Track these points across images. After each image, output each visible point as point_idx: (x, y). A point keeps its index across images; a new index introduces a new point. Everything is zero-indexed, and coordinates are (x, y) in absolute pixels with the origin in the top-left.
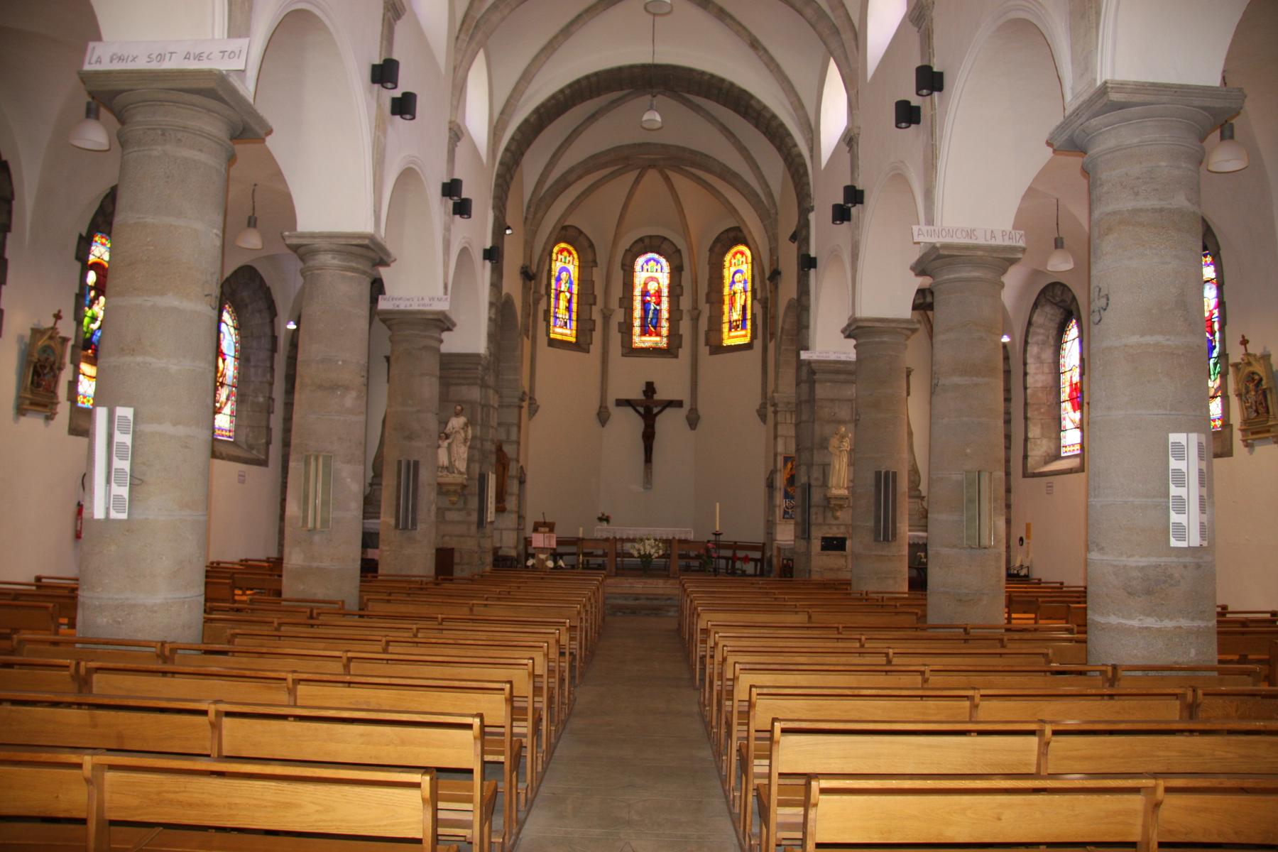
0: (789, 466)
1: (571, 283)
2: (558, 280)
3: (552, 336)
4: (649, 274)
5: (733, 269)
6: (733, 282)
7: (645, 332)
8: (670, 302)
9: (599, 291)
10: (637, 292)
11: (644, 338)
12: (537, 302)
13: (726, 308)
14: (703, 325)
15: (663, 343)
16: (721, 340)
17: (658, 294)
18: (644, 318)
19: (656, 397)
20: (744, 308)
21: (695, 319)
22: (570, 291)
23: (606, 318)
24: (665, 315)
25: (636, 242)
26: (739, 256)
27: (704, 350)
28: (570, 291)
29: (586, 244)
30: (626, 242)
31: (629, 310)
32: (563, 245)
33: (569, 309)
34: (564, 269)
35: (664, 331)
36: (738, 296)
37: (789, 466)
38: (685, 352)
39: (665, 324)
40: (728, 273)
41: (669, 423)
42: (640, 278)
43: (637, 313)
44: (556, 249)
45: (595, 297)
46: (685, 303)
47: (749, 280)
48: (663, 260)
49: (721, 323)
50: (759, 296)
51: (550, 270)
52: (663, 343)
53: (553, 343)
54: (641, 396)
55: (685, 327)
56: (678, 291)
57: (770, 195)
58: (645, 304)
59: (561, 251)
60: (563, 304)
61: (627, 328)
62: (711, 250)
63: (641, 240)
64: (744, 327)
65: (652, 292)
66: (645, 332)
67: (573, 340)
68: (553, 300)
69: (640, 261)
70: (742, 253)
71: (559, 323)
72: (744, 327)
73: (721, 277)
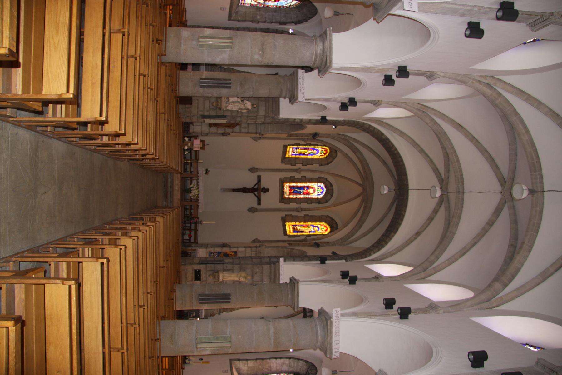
0: (233, 254)
2: (313, 149)
3: (288, 147)
4: (316, 189)
5: (319, 226)
6: (314, 226)
8: (304, 199)
9: (309, 167)
10: (309, 184)
12: (303, 140)
14: (295, 214)
15: (286, 196)
16: (288, 222)
17: (308, 193)
18: (297, 187)
19: (262, 193)
20: (302, 232)
22: (309, 154)
23: (297, 171)
24: (299, 197)
25: (331, 183)
26: (325, 229)
27: (283, 214)
28: (309, 154)
29: (329, 161)
30: (330, 179)
31: (301, 181)
32: (328, 151)
33: (301, 154)
34: (318, 151)
35: (291, 196)
36: (308, 229)
37: (233, 254)
38: (282, 206)
39: (295, 196)
40: (317, 224)
41: (250, 200)
42: (315, 185)
43: (299, 184)
44: (327, 148)
46: (304, 205)
48: (322, 195)
50: (307, 238)
51: (317, 145)
52: (286, 196)
53: (285, 147)
55: (293, 205)
57: (352, 242)
58: (303, 188)
59: (326, 150)
60: (303, 151)
61: (292, 180)
62: (328, 216)
64: (294, 232)
66: (291, 188)
67: (287, 156)
69: (322, 185)
70: (327, 230)
71: (294, 150)
72: (294, 232)
73: (316, 221)
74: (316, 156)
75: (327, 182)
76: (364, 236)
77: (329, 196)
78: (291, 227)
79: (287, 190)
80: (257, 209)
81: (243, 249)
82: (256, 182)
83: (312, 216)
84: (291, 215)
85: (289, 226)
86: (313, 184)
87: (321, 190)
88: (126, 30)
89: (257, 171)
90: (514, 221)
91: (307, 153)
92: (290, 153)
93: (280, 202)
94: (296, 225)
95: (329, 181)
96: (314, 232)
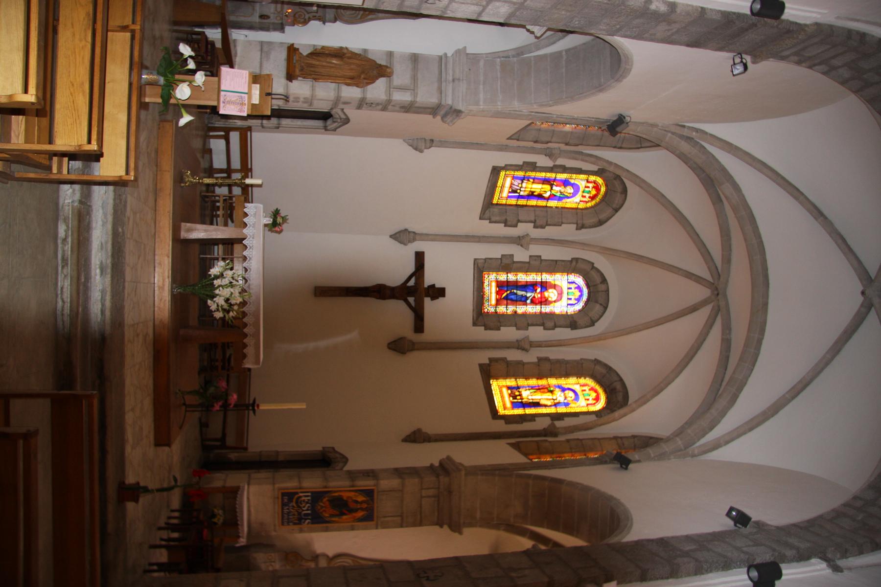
0: (361, 498)
1: (560, 199)
2: (566, 183)
3: (502, 174)
4: (565, 291)
5: (577, 388)
6: (563, 390)
7: (501, 286)
8: (535, 315)
9: (550, 232)
10: (546, 277)
11: (494, 284)
12: (550, 154)
13: (533, 382)
14: (513, 355)
15: (489, 308)
16: (497, 378)
17: (544, 301)
18: (516, 285)
19: (427, 300)
20: (537, 404)
21: (518, 345)
22: (552, 197)
23: (519, 241)
24: (521, 309)
25: (602, 275)
26: (594, 395)
27: (484, 357)
28: (552, 197)
29: (603, 216)
30: (602, 263)
31: (526, 268)
32: (603, 189)
33: (531, 195)
34: (576, 188)
35: (502, 309)
36: (548, 396)
37: (361, 498)
38: (480, 334)
39: (511, 309)
40: (571, 382)
41: (397, 314)
42: (560, 279)
43: (522, 277)
44: (600, 180)
45: (543, 227)
46: (536, 333)
47: (568, 410)
48: (579, 306)
49: (516, 376)
50: (558, 424)
51: (579, 171)
52: (489, 308)
53: (496, 171)
54: (427, 282)
55: (509, 333)
56: (550, 324)
57: (716, 445)
58: (532, 286)
59: (597, 188)
60: (537, 188)
61: (506, 264)
62: (597, 362)
63: (604, 280)
64: (515, 405)
65: (546, 294)
66: (501, 286)
67: (495, 202)
68: (543, 175)
69: (580, 281)
70: (597, 399)
71: (517, 182)
72: (515, 405)
73: (567, 375)
74: (570, 203)
75: (593, 273)
76: (751, 429)
77: (598, 308)
78: (504, 390)
79: (491, 291)
80: (413, 344)
81: (395, 483)
82: (411, 268)
83: (558, 361)
84: (504, 360)
85: (500, 388)
86: (558, 276)
87: (578, 294)
88: (137, 27)
89: (414, 240)
90: (726, 343)
91: (547, 195)
92: (505, 194)
93: (475, 324)
94: (518, 388)
95: (598, 271)
96: (567, 405)
